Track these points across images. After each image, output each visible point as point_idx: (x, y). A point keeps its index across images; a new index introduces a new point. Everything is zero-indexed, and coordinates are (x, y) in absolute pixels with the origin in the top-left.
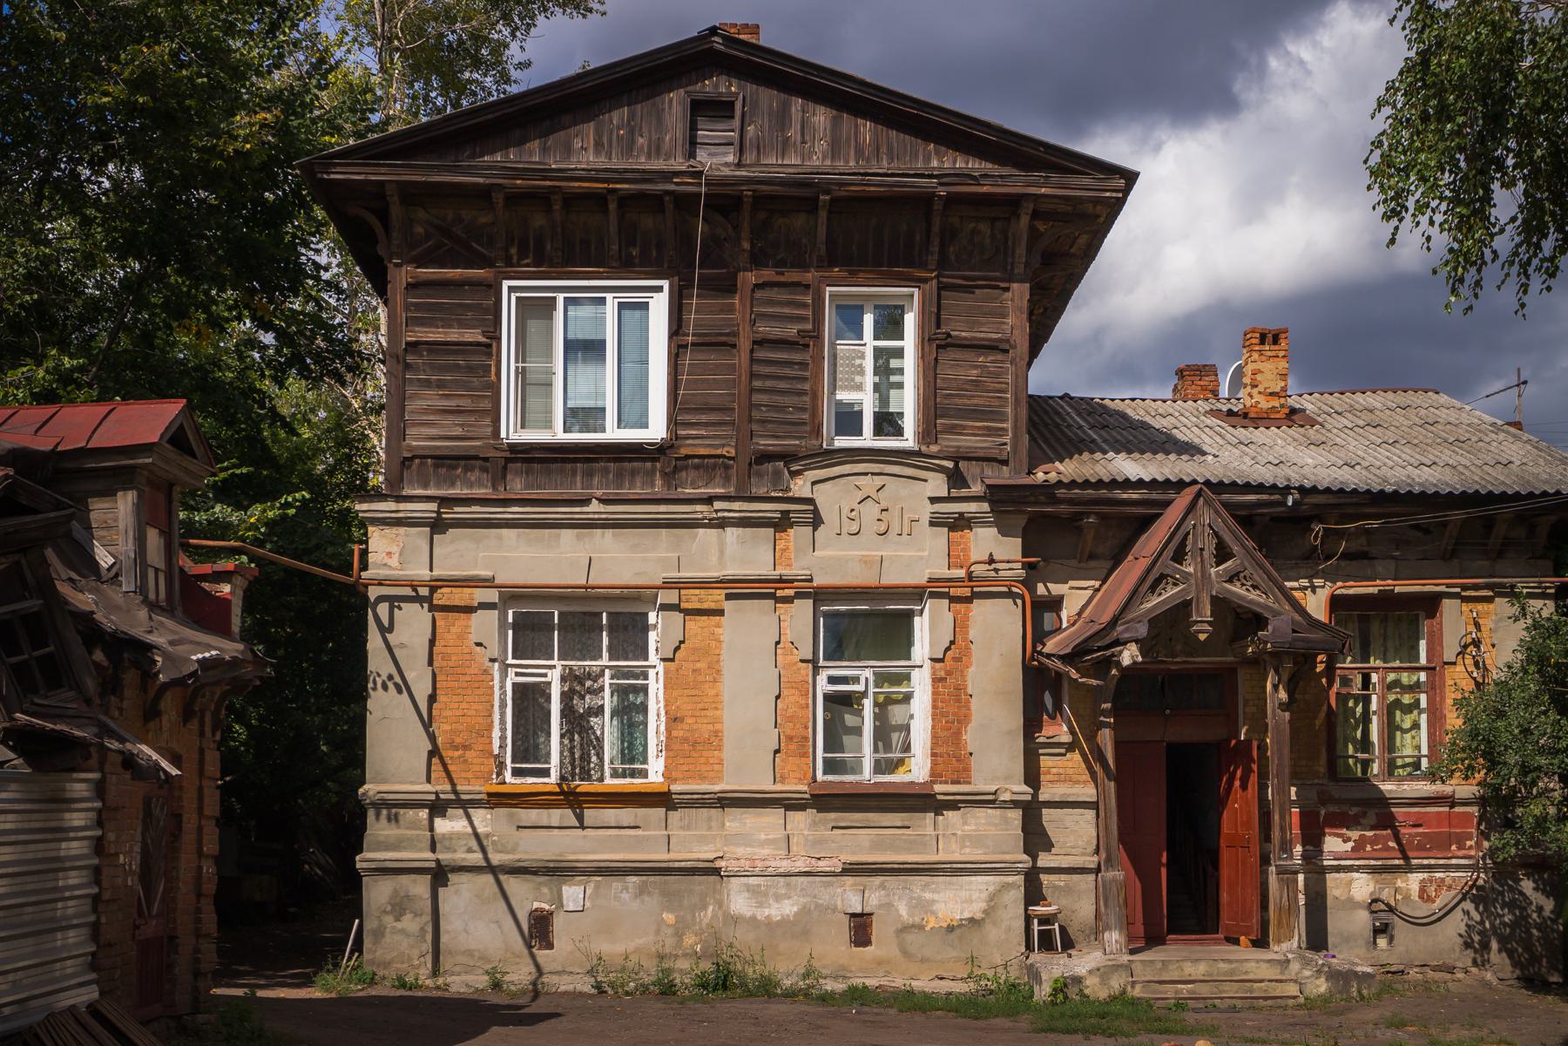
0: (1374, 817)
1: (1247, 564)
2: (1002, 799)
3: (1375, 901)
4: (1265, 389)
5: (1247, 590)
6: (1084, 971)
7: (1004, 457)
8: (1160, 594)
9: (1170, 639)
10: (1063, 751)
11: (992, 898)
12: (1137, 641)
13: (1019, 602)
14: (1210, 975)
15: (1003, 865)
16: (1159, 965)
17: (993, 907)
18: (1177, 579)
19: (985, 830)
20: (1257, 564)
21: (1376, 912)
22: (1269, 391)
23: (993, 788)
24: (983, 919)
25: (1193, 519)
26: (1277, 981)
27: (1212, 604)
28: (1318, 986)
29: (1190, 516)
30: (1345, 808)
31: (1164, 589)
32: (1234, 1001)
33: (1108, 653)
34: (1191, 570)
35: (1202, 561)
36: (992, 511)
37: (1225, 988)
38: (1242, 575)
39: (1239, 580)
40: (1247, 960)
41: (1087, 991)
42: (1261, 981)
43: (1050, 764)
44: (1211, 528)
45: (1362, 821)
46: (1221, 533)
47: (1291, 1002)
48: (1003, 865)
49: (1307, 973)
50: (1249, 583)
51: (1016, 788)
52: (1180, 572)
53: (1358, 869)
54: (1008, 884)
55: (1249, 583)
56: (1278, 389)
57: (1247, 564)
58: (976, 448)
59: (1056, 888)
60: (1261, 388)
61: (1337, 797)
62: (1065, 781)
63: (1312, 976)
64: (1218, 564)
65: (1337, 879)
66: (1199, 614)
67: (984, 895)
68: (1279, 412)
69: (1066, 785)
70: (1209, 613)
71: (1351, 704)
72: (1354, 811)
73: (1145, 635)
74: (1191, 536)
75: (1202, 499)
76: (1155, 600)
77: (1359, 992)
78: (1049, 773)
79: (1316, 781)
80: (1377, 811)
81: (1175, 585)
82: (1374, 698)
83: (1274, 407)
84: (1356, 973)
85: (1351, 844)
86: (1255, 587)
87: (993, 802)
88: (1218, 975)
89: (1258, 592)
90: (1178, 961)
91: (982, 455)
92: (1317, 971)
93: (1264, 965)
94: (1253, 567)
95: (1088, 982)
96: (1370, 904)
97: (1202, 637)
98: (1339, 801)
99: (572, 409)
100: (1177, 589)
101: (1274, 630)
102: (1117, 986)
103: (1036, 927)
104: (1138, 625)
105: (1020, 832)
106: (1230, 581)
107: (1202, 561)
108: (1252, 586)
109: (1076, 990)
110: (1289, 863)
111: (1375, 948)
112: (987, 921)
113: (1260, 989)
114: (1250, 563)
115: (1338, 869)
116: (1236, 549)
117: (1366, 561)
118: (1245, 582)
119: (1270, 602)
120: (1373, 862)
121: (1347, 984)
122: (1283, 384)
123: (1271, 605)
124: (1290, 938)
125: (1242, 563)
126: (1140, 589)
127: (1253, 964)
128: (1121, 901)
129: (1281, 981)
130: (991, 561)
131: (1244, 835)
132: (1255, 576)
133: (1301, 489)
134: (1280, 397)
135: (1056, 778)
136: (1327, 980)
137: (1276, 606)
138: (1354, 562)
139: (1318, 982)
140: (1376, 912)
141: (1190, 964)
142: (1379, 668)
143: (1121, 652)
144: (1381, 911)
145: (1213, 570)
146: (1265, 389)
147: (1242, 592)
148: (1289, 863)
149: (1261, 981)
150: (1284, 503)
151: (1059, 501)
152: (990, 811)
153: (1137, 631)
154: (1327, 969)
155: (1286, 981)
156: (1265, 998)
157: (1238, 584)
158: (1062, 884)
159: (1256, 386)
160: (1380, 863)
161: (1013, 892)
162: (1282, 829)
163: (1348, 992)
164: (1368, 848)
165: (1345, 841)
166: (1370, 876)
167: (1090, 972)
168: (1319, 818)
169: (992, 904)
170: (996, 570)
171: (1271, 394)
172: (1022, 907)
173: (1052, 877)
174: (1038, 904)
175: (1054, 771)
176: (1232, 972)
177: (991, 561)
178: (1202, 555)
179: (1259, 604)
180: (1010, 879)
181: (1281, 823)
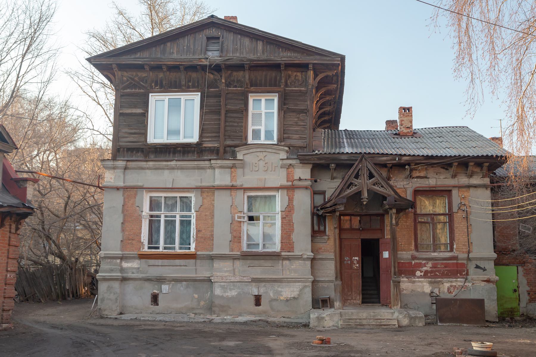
0: (431, 264)
4: (405, 126)
11: (301, 290)
18: (356, 184)
22: (406, 127)
23: (301, 254)
26: (389, 319)
28: (405, 321)
29: (360, 164)
30: (421, 261)
31: (352, 187)
39: (377, 184)
42: (384, 319)
48: (304, 279)
51: (308, 254)
52: (356, 182)
54: (306, 286)
60: (404, 126)
70: (367, 195)
72: (424, 262)
80: (432, 262)
81: (356, 186)
86: (382, 187)
89: (383, 188)
100: (356, 188)
108: (381, 186)
118: (379, 185)
122: (411, 124)
129: (391, 319)
152: (300, 261)
157: (377, 185)
158: (326, 286)
159: (402, 125)
164: (429, 275)
165: (421, 272)
171: (407, 128)
178: (364, 176)
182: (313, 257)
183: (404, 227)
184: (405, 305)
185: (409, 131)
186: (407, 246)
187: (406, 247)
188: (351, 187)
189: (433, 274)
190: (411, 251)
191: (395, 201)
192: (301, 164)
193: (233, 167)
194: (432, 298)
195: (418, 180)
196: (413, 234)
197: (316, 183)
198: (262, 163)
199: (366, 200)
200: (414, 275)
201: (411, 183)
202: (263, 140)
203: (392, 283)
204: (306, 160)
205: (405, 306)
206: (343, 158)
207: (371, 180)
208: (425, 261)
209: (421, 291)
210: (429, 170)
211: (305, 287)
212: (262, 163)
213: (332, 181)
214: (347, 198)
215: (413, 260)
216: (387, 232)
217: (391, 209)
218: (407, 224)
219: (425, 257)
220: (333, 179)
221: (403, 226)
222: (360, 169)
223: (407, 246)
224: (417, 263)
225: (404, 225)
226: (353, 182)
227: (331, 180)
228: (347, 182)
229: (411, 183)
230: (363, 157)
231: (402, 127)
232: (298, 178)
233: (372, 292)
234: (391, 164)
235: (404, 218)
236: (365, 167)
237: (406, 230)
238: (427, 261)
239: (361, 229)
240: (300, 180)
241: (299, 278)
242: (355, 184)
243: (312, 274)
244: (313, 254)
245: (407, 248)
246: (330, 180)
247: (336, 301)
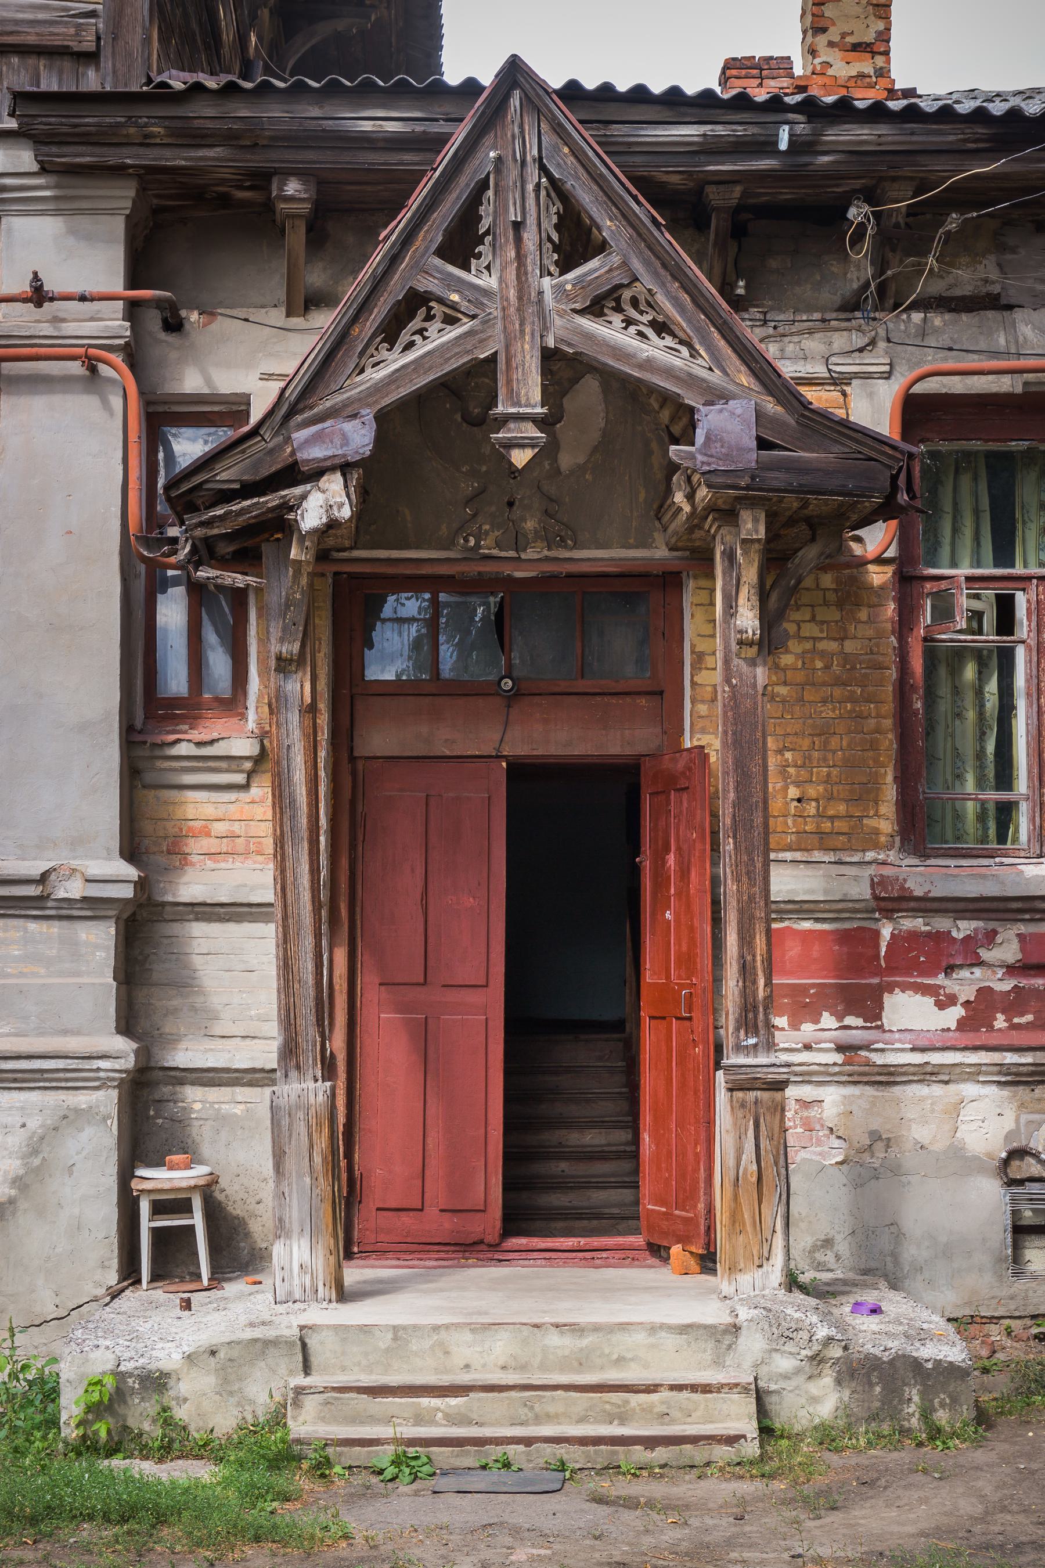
0: (1015, 945)
1: (637, 265)
2: (62, 894)
3: (1018, 1154)
4: (843, 35)
5: (640, 334)
6: (177, 1356)
7: (90, 46)
8: (410, 345)
9: (511, 504)
10: (240, 778)
11: (34, 1148)
12: (345, 468)
13: (117, 402)
14: (523, 1368)
15: (60, 1064)
16: (385, 1340)
17: (37, 1171)
18: (453, 306)
19: (22, 975)
20: (664, 266)
21: (1021, 1182)
22: (849, 40)
23: (34, 868)
24: (12, 1201)
25: (495, 147)
26: (694, 1388)
27: (546, 371)
28: (814, 1400)
29: (488, 140)
30: (942, 923)
31: (421, 332)
32: (562, 1451)
33: (271, 500)
34: (490, 282)
35: (520, 257)
36: (44, 169)
37: (551, 1409)
38: (627, 294)
39: (619, 309)
40: (624, 1327)
41: (181, 1413)
42: (651, 1389)
43: (209, 811)
44: (543, 169)
45: (985, 954)
46: (570, 184)
47: (722, 1453)
48: (60, 1064)
49: (784, 1363)
50: (645, 318)
51: (97, 868)
52: (461, 286)
53: (974, 1074)
54: (77, 1111)
55: (645, 318)
56: (870, 37)
57: (637, 265)
58: (17, 22)
59: (223, 1120)
60: (834, 35)
61: (918, 892)
62: (246, 854)
63: (798, 1371)
64: (565, 267)
65: (922, 1099)
66: (514, 399)
67: (16, 1140)
68: (872, 86)
69: (249, 864)
70: (537, 395)
71: (970, 672)
72: (964, 928)
73: (367, 451)
74: (490, 193)
75: (517, 94)
76: (395, 361)
77: (926, 1414)
78: (208, 835)
79: (870, 855)
80: (1022, 928)
81: (451, 321)
82: (1020, 652)
83: (862, 76)
84: (916, 1365)
85: (957, 1012)
86: (661, 328)
87: (41, 900)
88: (543, 1367)
89: (669, 341)
90: (436, 1328)
91: (31, 39)
92: (812, 1358)
93: (670, 1341)
94: (656, 274)
95: (184, 1387)
96: (1006, 1162)
97: (520, 458)
98: (928, 905)
99: (997, 784)
100: (454, 333)
101: (708, 438)
102: (263, 1398)
103: (146, 1224)
104: (348, 427)
105: (110, 980)
106: (595, 309)
107: (520, 257)
108: (653, 324)
109: (151, 1407)
110: (762, 1059)
111: (1018, 1273)
112: (22, 1205)
113: (647, 1410)
114: (647, 263)
115: (927, 1074)
116: (608, 226)
117: (990, 314)
118: (633, 314)
119: (699, 369)
120: (1010, 1058)
121: (893, 1394)
122: (881, 26)
123: (704, 374)
124: (763, 1260)
125: (625, 264)
126: (356, 330)
127: (640, 1337)
128: (318, 1159)
129: (706, 1389)
130: (38, 295)
131: (682, 987)
132: (661, 298)
133: (810, 108)
134: (874, 53)
135: (225, 846)
136: (839, 1382)
137: (716, 378)
138: (964, 317)
139: (814, 1388)
140: (1021, 1182)
141: (468, 1336)
142: (1029, 578)
143: (304, 497)
144: (1033, 1180)
145: (547, 282)
146: (843, 35)
147: (627, 340)
148: (762, 1059)
149: (651, 1389)
150: (768, 147)
151: (197, 138)
152: (33, 926)
153: (345, 440)
154: (836, 1352)
155: (720, 1388)
156: (651, 1442)
157: (617, 319)
158: (238, 1110)
159: (824, 30)
160: (1028, 1058)
161: (89, 1132)
162: (746, 971)
163: (895, 1415)
164: (1000, 1022)
165: (941, 1005)
166: (1006, 1092)
167: (190, 1358)
168: (877, 946)
169: (36, 1161)
170: (56, 320)
171: (856, 47)
172: (112, 1170)
173: (214, 1094)
174: (159, 1163)
175: (219, 828)
176: (581, 1363)
177: (38, 295)
178: (518, 241)
179: (669, 372)
180: (82, 1099)
181: (742, 956)
182: (127, 892)
183: (827, 667)
184: (815, 1248)
185: (869, 70)
186: (842, 808)
187: (832, 818)
188: (416, 324)
189: (1029, 1018)
190: (876, 846)
191: (763, 444)
192: (51, 179)
194: (1016, 1190)
195: (937, 320)
196: (888, 723)
197: (171, 338)
199: (532, 432)
200: (978, 1030)
201: (882, 345)
203: (722, 1097)
204: (85, 139)
205: (819, 1256)
206: (367, 126)
207: (570, 276)
208: (974, 924)
209: (938, 1147)
210: (1013, 250)
211: (70, 1118)
213: (296, 322)
214: (377, 418)
215: (888, 913)
216: (703, 709)
217: (729, 515)
218: (849, 646)
219: (972, 889)
220: (307, 309)
221: (819, 664)
222: (483, 185)
223: (842, 808)
224: (914, 936)
225: (823, 654)
226: (426, 284)
227: (288, 315)
228: (379, 282)
229: (882, 345)
230: (515, 85)
231: (822, 40)
232: (23, 286)
233: (592, 1138)
234: (738, 190)
235: (826, 603)
236: (533, 174)
237: (837, 692)
238: (992, 925)
239: (507, 684)
240: (39, 304)
241: (18, 1057)
242: (441, 301)
243: (127, 1025)
244: (131, 872)
245: (841, 825)
246: (277, 316)
247: (281, 1229)
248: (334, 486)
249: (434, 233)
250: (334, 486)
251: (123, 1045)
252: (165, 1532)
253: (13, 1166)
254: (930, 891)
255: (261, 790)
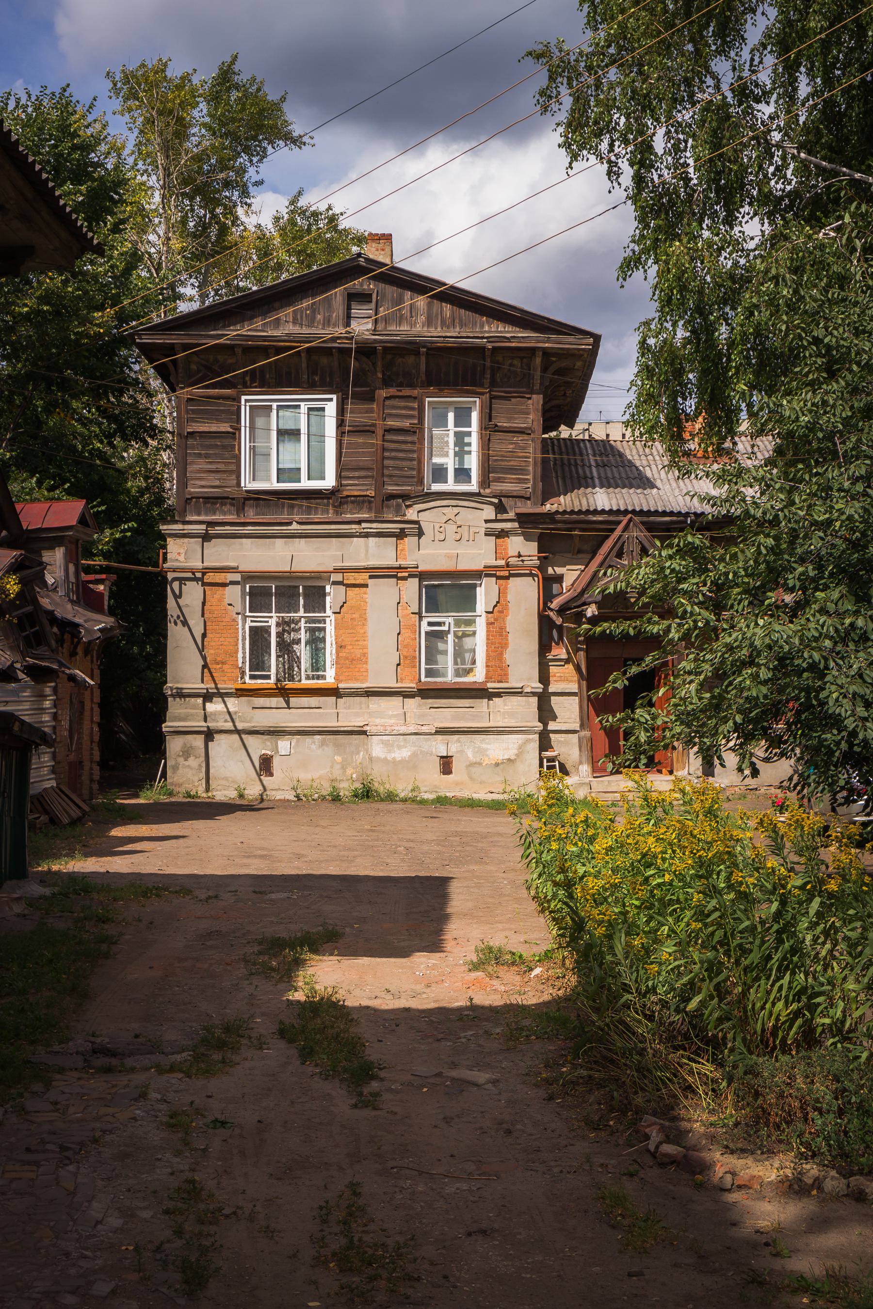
12: (596, 603)
67: (516, 746)
97: (633, 600)
124: (684, 768)
130: (519, 556)
173: (557, 736)
177: (519, 556)
180: (531, 736)
193: (401, 535)
198: (451, 528)
202: (451, 485)
211: (528, 741)
212: (451, 528)
248: (594, 606)
249: (614, 552)
250: (594, 606)
251: (540, 724)
252: (828, 678)
253: (516, 751)
254: (723, 766)
255: (570, 666)
